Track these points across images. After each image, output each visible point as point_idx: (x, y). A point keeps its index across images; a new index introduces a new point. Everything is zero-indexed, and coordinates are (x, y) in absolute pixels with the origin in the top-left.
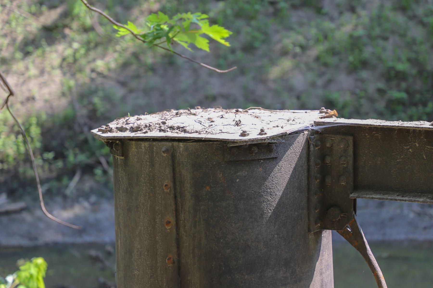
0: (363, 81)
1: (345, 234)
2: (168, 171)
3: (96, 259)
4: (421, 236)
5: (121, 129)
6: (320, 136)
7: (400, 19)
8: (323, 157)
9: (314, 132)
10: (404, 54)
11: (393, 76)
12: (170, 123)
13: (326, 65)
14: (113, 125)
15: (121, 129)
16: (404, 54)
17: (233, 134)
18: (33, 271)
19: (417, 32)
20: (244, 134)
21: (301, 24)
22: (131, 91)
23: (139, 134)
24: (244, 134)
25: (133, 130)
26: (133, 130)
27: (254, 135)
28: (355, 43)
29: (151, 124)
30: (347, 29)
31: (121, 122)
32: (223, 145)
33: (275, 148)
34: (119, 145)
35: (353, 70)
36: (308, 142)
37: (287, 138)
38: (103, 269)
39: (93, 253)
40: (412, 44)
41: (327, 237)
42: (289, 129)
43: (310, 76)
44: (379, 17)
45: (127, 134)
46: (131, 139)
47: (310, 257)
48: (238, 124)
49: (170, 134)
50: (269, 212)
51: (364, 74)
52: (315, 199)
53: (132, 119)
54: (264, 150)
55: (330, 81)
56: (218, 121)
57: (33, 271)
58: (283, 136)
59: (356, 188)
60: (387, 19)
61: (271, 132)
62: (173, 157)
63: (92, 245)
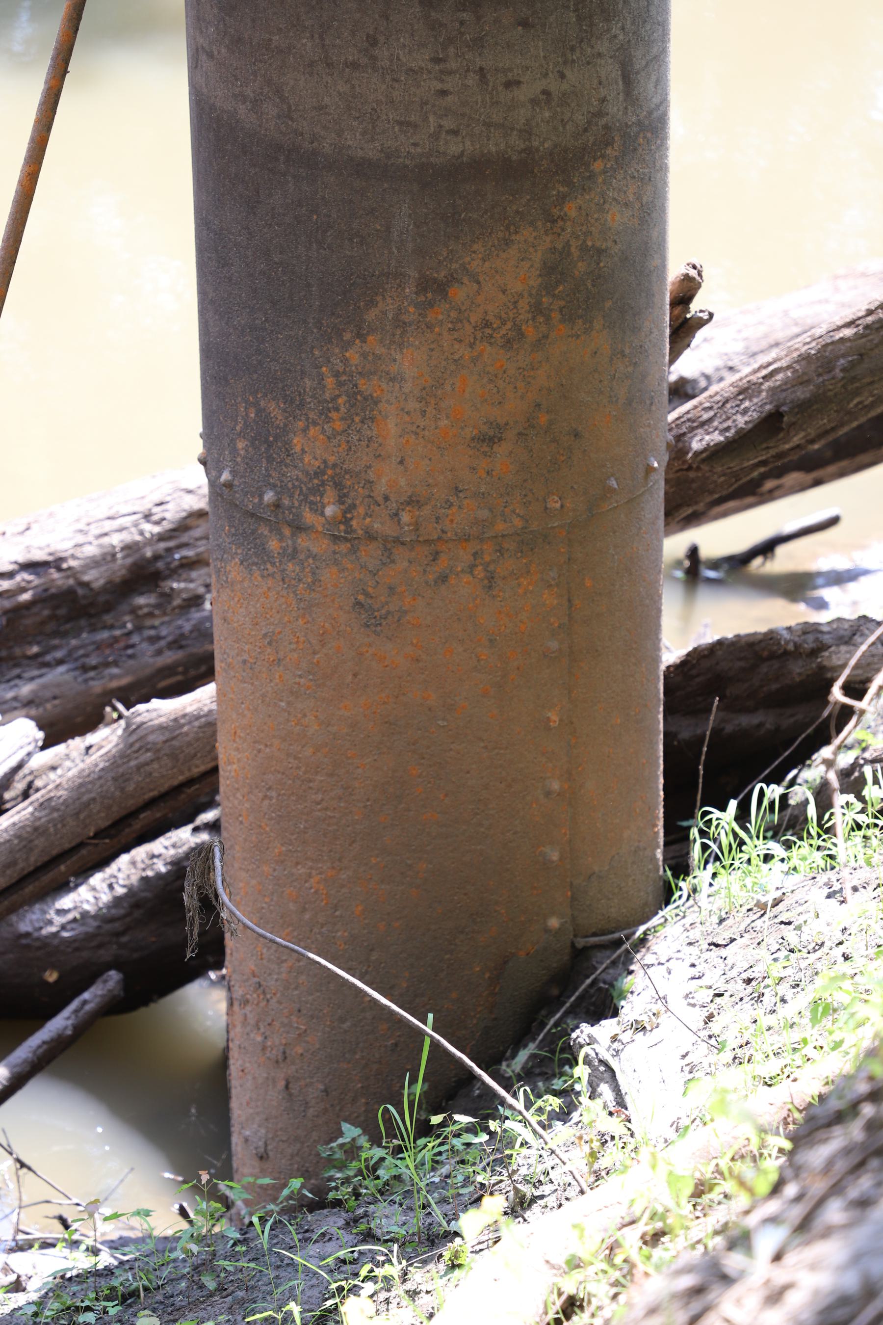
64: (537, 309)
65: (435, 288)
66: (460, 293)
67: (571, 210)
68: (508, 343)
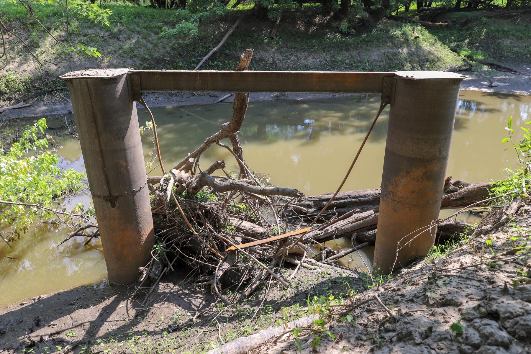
0: (135, 61)
1: (139, 102)
2: (86, 87)
3: (59, 119)
4: (156, 106)
5: (69, 76)
6: (130, 76)
7: (145, 42)
8: (131, 82)
9: (128, 74)
10: (147, 53)
11: (144, 60)
12: (84, 73)
13: (123, 57)
14: (66, 74)
15: (69, 76)
16: (147, 53)
17: (105, 76)
18: (42, 122)
19: (150, 46)
20: (108, 75)
21: (113, 44)
22: (59, 67)
23: (75, 77)
24: (108, 75)
25: (73, 76)
26: (73, 76)
27: (111, 76)
28: (131, 50)
29: (78, 74)
30: (128, 46)
31: (69, 74)
32: (102, 79)
33: (58, 98)
34: (70, 80)
35: (131, 58)
36: (126, 77)
37: (121, 76)
38: (61, 122)
39: (57, 117)
40: (149, 49)
41: (134, 103)
42: (121, 73)
43: (118, 60)
44: (138, 41)
45: (71, 77)
46: (73, 78)
47: (131, 109)
48: (105, 73)
49: (85, 76)
50: (118, 97)
51: (135, 59)
52: (130, 93)
53: (72, 73)
54: (114, 80)
55: (125, 62)
56: (99, 72)
57: (42, 122)
58: (119, 75)
59: (141, 89)
60: (141, 42)
61: (116, 75)
62: (87, 83)
63: (55, 115)
64: (422, 178)
65: (408, 172)
66: (411, 174)
67: (429, 166)
68: (417, 181)
